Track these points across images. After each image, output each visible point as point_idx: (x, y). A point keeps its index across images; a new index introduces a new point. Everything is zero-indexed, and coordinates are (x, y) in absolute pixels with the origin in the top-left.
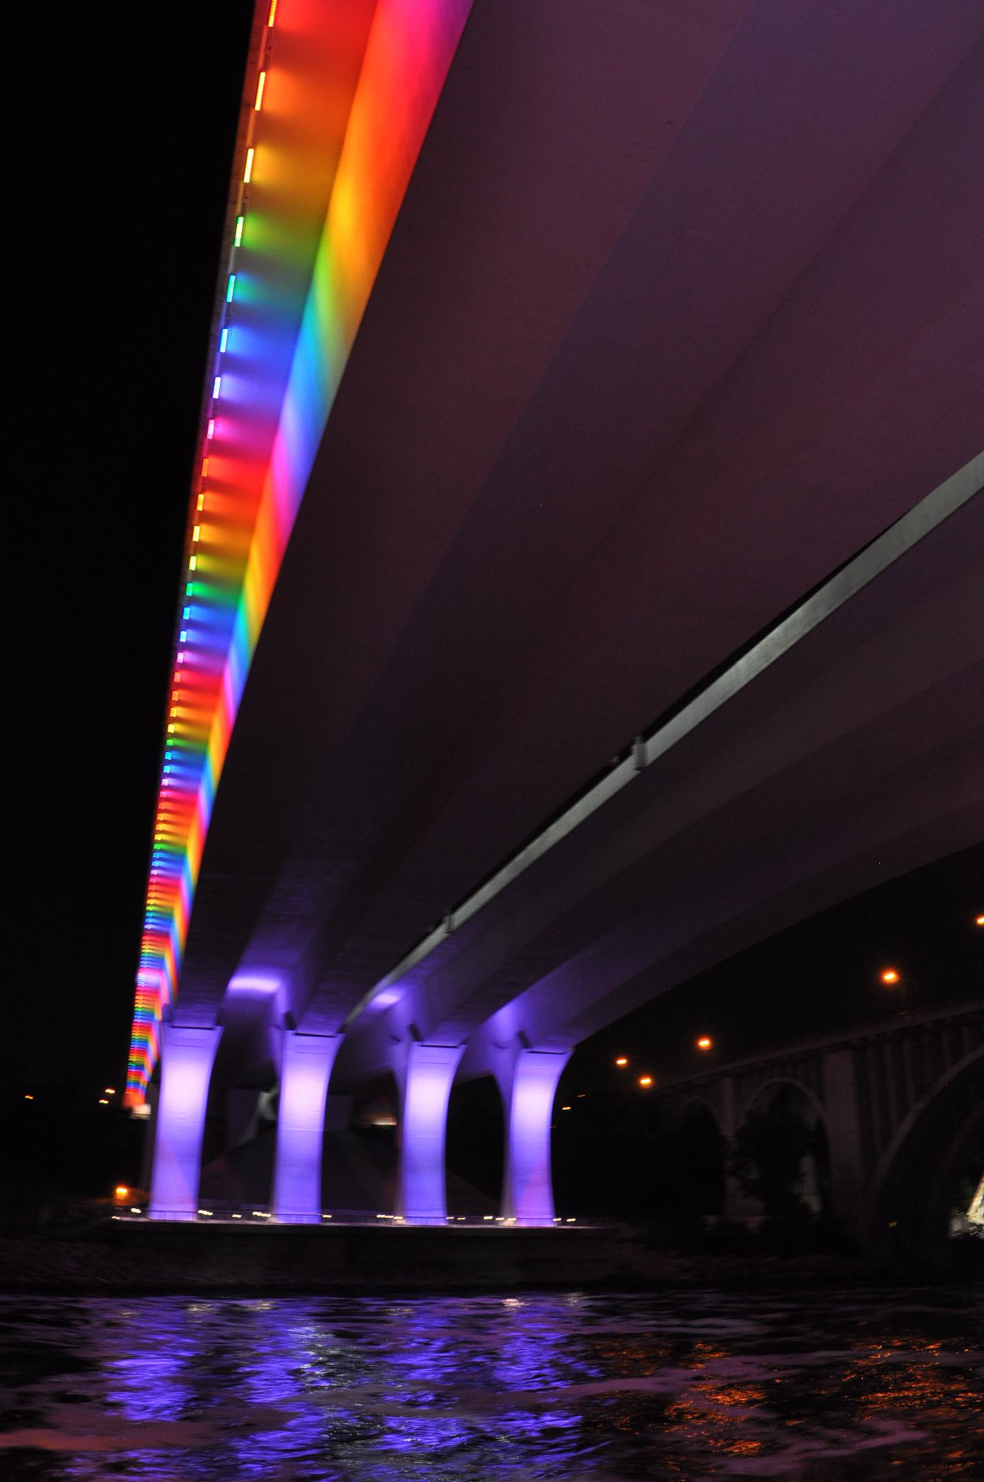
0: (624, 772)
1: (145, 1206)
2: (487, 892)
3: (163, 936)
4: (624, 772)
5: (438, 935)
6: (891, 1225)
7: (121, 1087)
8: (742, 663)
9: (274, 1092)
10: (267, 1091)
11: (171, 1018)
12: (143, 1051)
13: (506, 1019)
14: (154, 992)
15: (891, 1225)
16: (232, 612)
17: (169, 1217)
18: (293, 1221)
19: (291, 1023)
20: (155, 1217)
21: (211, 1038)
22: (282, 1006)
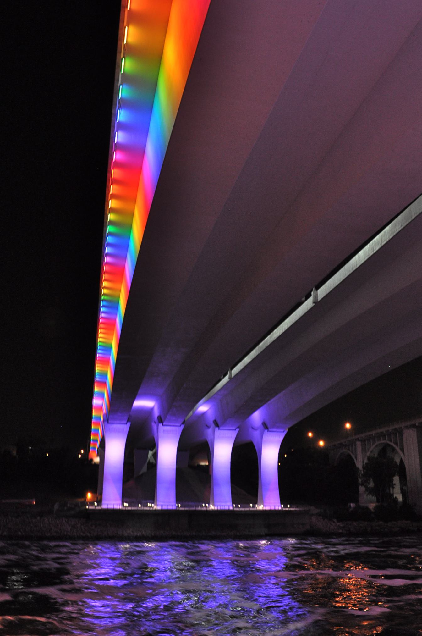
0: (308, 304)
1: (99, 502)
2: (247, 360)
3: (103, 383)
4: (308, 304)
5: (226, 379)
6: (30, 449)
7: (87, 450)
8: (361, 253)
9: (154, 450)
10: (152, 450)
11: (107, 419)
12: (96, 434)
13: (257, 416)
14: (100, 408)
15: (30, 449)
16: (127, 239)
17: (110, 507)
18: (165, 508)
19: (161, 420)
20: (104, 507)
21: (126, 428)
22: (156, 413)
